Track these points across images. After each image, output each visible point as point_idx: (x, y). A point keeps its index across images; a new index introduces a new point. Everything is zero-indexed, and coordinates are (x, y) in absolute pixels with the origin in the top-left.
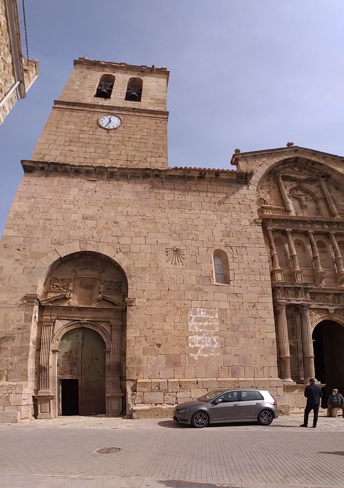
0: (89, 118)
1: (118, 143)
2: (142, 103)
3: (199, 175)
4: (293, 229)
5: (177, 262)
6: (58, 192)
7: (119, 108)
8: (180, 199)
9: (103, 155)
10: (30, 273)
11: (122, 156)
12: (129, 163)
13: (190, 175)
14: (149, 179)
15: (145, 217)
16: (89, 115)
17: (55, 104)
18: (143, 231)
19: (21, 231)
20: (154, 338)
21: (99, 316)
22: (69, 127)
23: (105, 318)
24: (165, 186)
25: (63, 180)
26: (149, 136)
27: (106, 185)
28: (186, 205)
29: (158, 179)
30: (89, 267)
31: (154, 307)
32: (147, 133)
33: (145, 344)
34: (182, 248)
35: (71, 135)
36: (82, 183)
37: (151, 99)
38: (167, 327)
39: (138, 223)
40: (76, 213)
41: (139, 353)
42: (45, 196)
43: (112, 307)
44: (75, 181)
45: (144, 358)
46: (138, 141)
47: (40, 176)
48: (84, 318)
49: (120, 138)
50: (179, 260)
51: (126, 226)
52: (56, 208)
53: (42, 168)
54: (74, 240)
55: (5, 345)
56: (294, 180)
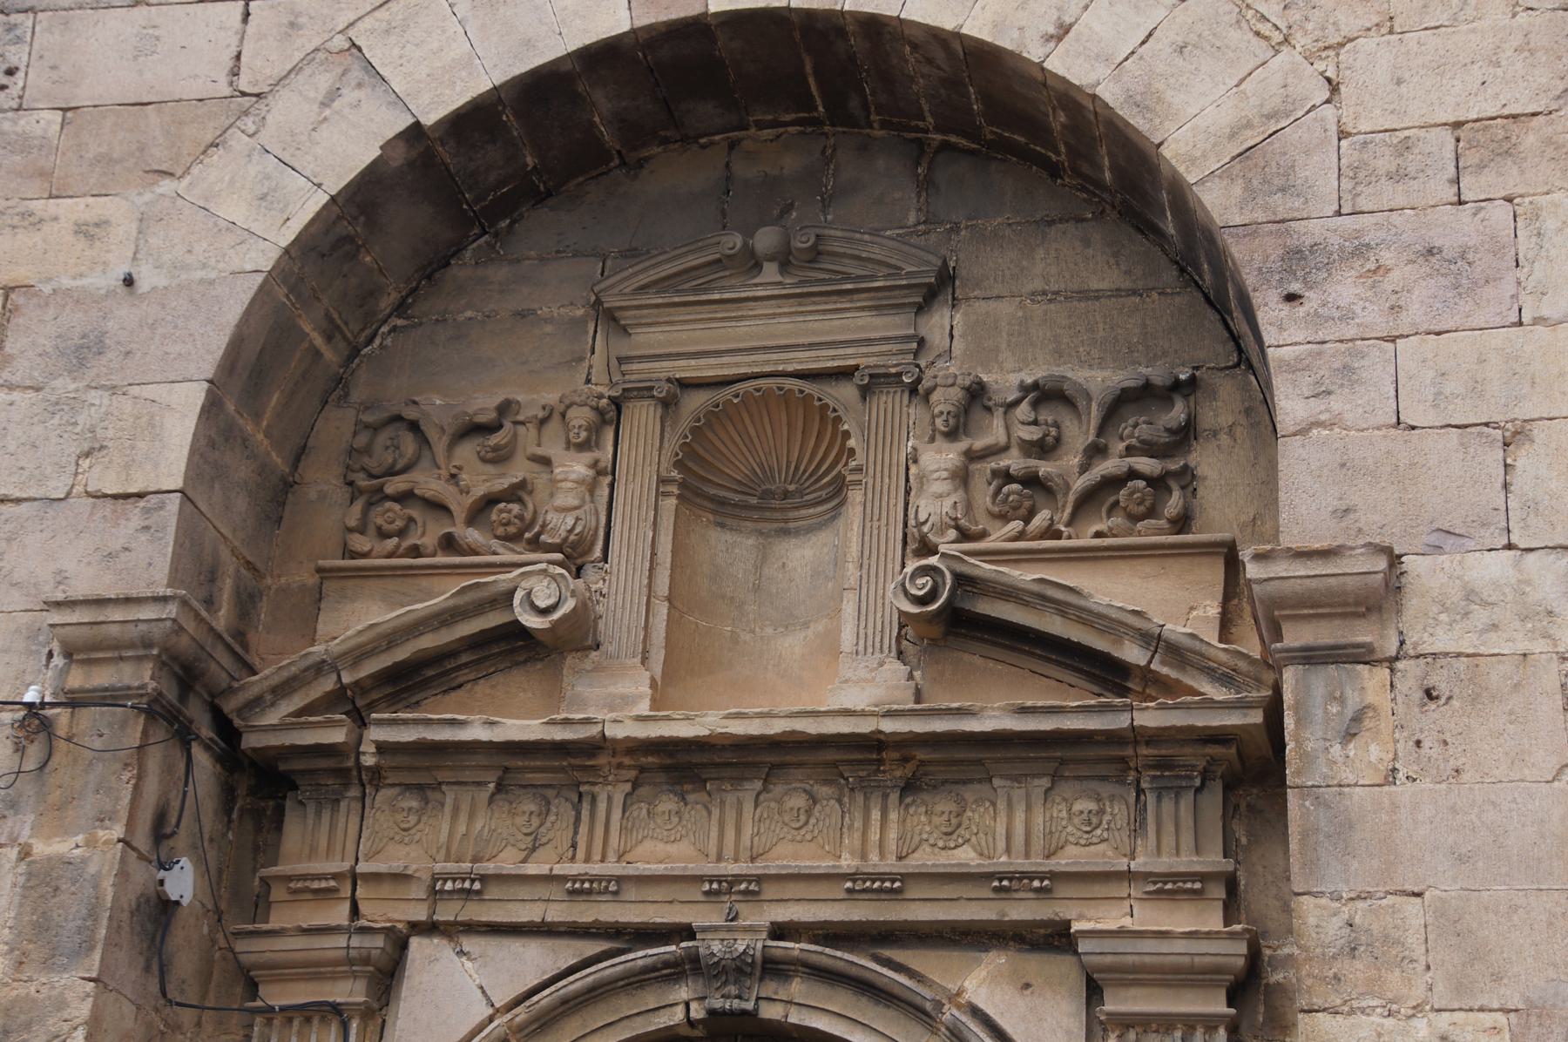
10: (83, 352)
21: (926, 859)
23: (1005, 883)
30: (766, 239)
43: (1074, 709)
48: (752, 888)
55: (1554, 763)
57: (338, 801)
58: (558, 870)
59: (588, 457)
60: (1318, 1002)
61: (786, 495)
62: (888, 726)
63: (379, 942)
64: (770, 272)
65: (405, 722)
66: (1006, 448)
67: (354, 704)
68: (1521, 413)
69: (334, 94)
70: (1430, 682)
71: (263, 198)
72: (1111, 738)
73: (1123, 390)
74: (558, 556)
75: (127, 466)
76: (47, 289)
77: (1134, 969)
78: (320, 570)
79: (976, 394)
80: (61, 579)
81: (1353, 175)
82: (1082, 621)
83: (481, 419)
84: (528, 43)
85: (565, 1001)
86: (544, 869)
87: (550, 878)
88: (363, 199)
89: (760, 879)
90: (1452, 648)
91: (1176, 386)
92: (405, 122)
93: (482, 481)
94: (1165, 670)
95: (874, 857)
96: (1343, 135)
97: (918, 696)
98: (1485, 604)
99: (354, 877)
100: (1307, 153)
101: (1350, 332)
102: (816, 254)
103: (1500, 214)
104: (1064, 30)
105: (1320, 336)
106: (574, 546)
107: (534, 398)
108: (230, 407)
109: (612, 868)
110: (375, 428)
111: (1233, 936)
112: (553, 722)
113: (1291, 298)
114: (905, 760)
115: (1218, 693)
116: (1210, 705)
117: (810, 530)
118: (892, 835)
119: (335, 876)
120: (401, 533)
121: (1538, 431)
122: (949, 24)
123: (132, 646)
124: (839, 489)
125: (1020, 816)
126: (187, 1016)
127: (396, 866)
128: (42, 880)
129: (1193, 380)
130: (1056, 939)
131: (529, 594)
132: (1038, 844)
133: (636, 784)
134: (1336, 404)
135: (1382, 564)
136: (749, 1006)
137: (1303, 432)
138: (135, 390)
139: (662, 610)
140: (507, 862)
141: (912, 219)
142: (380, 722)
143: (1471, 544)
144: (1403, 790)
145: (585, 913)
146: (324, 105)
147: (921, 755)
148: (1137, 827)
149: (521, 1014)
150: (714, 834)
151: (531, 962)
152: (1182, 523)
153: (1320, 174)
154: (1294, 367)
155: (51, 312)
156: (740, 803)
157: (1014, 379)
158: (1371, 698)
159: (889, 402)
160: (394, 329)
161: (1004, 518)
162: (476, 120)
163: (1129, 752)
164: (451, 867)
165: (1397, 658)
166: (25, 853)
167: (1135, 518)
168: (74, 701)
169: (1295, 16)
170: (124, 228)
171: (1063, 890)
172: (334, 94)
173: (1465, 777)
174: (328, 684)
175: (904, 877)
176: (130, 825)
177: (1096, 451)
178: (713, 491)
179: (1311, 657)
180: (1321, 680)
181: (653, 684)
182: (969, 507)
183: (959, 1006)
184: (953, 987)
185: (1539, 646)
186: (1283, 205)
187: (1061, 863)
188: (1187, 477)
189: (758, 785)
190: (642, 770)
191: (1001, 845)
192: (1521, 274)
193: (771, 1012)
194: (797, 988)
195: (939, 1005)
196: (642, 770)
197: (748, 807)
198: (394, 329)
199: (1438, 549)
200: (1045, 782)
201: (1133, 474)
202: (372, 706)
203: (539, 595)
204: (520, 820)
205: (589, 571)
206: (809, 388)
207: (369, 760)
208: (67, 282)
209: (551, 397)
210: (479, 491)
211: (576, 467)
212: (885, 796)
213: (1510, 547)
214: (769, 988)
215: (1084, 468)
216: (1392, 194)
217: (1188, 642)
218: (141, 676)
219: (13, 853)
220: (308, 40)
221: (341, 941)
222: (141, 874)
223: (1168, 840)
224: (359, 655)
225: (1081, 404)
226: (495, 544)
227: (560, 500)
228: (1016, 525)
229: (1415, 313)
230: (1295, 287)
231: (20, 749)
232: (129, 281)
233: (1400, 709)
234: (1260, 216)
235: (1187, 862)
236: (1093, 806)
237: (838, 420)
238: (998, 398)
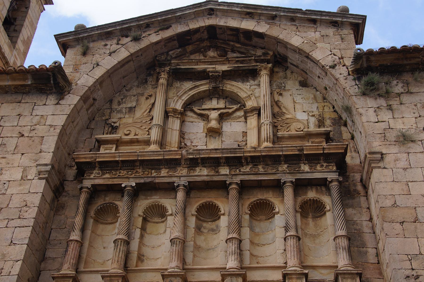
4: (138, 181)
56: (203, 75)
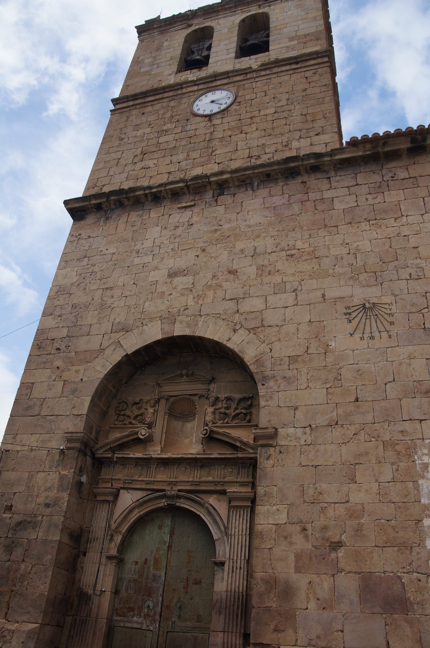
0: (173, 107)
1: (229, 133)
2: (271, 52)
3: (409, 145)
5: (376, 334)
6: (124, 240)
7: (226, 75)
8: (371, 201)
9: (203, 159)
10: (74, 391)
11: (239, 153)
12: (253, 160)
13: (388, 149)
14: (300, 179)
15: (293, 252)
16: (172, 104)
17: (114, 105)
18: (291, 279)
19: (64, 316)
20: (325, 528)
21: (204, 479)
22: (139, 133)
23: (216, 483)
24: (334, 184)
25: (134, 219)
26: (292, 103)
27: (210, 209)
28: (386, 211)
29: (319, 175)
30: (184, 372)
31: (322, 448)
32: (288, 99)
33: (300, 543)
34: (387, 299)
35: (144, 144)
36: (166, 217)
37: (291, 39)
38: (358, 497)
39: (279, 266)
40: (156, 268)
41: (286, 570)
42: (104, 251)
43: (228, 453)
44: (155, 213)
45: (301, 581)
46: (270, 118)
47: (96, 222)
49: (233, 123)
50: (382, 328)
51: (253, 277)
52: (123, 268)
53: (99, 207)
54: (151, 319)
57: (110, 466)
58: (144, 479)
59: (153, 408)
60: (259, 504)
61: (187, 415)
62: (198, 456)
63: (115, 490)
64: (185, 377)
65: (120, 453)
66: (222, 408)
67: (113, 450)
68: (297, 404)
69: (115, 349)
70: (281, 450)
71: (103, 366)
72: (234, 459)
73: (241, 398)
74: (147, 426)
75: (79, 410)
76: (70, 381)
77: (236, 498)
78: (110, 427)
79: (217, 399)
80: (68, 428)
81: (273, 364)
82: (230, 438)
83: (137, 402)
84: (146, 341)
85: (144, 501)
86: (142, 479)
87: (143, 481)
88: (119, 366)
89: (176, 482)
90: (284, 444)
91: (249, 398)
92: (125, 353)
93: (136, 412)
94: (243, 447)
95: (195, 478)
96: (272, 358)
97: (204, 451)
98: (290, 437)
99: (112, 479)
100: (267, 360)
101: (272, 390)
102: (192, 374)
103: (295, 371)
104: (230, 339)
105: (267, 391)
106: (150, 424)
107: (146, 398)
108: (96, 400)
109: (153, 479)
110: (120, 403)
111: (252, 492)
112: (144, 454)
113: (263, 385)
114: (201, 462)
115: (251, 451)
116: (250, 453)
117: (191, 421)
118: (198, 475)
119: (109, 479)
120: (123, 421)
121: (299, 408)
122: (212, 338)
123: (77, 440)
124: (195, 414)
125: (219, 472)
126: (85, 501)
127: (118, 478)
128: (62, 478)
129: (252, 397)
130: (223, 493)
131: (141, 432)
132: (222, 476)
133: (157, 465)
134: (269, 403)
135: (274, 430)
136: (174, 503)
137: (264, 407)
138: (81, 398)
139: (164, 435)
140: (136, 478)
141: (209, 368)
142: (116, 453)
143: (288, 427)
144: (275, 468)
145: (148, 487)
146: (113, 351)
147: (204, 461)
148: (238, 474)
149: (137, 503)
150: (169, 474)
151: (139, 495)
152: (249, 421)
153: (268, 364)
154: (263, 396)
155: (70, 385)
156: (174, 469)
157: (224, 396)
158: (271, 453)
159: (203, 400)
160: (125, 386)
161: (220, 420)
162: (137, 353)
163: (237, 461)
164: (127, 478)
165: (276, 446)
166: (60, 473)
167: (242, 420)
168: (68, 449)
169: (265, 338)
170: (82, 371)
171: (225, 485)
172: (115, 349)
173: (285, 466)
174: (109, 447)
175: (200, 482)
176: (75, 470)
177: (236, 409)
178: (175, 414)
179: (263, 446)
180: (264, 450)
181: (161, 448)
182: (215, 418)
183: (208, 504)
184: (207, 501)
185: (298, 444)
186: (263, 369)
187: (226, 480)
188: (251, 413)
189: (177, 466)
190: (158, 463)
191: (216, 476)
192: (298, 381)
193: (178, 504)
194: (182, 500)
195: (205, 504)
196: (158, 463)
197: (175, 469)
198: (125, 386)
199: (283, 427)
200: (224, 466)
201: (241, 413)
202: (116, 451)
203: (143, 433)
204: (139, 471)
205: (153, 428)
206: (191, 397)
207: (115, 460)
208: (73, 380)
209: (148, 398)
210: (135, 414)
211: (151, 410)
212: (198, 468)
213: (294, 427)
214: (177, 500)
215: (234, 412)
216: (279, 368)
217: (247, 442)
218: (78, 445)
219: (58, 473)
220: (112, 340)
221: (109, 490)
222: (77, 478)
223: (243, 476)
224: (114, 442)
225: (234, 401)
226: (137, 423)
227: (148, 416)
228: (222, 421)
229: (282, 388)
230: (264, 383)
231: (60, 456)
232: (82, 380)
233: (276, 455)
234: (259, 371)
235: (246, 480)
236: (231, 470)
237: (195, 403)
238: (221, 399)
